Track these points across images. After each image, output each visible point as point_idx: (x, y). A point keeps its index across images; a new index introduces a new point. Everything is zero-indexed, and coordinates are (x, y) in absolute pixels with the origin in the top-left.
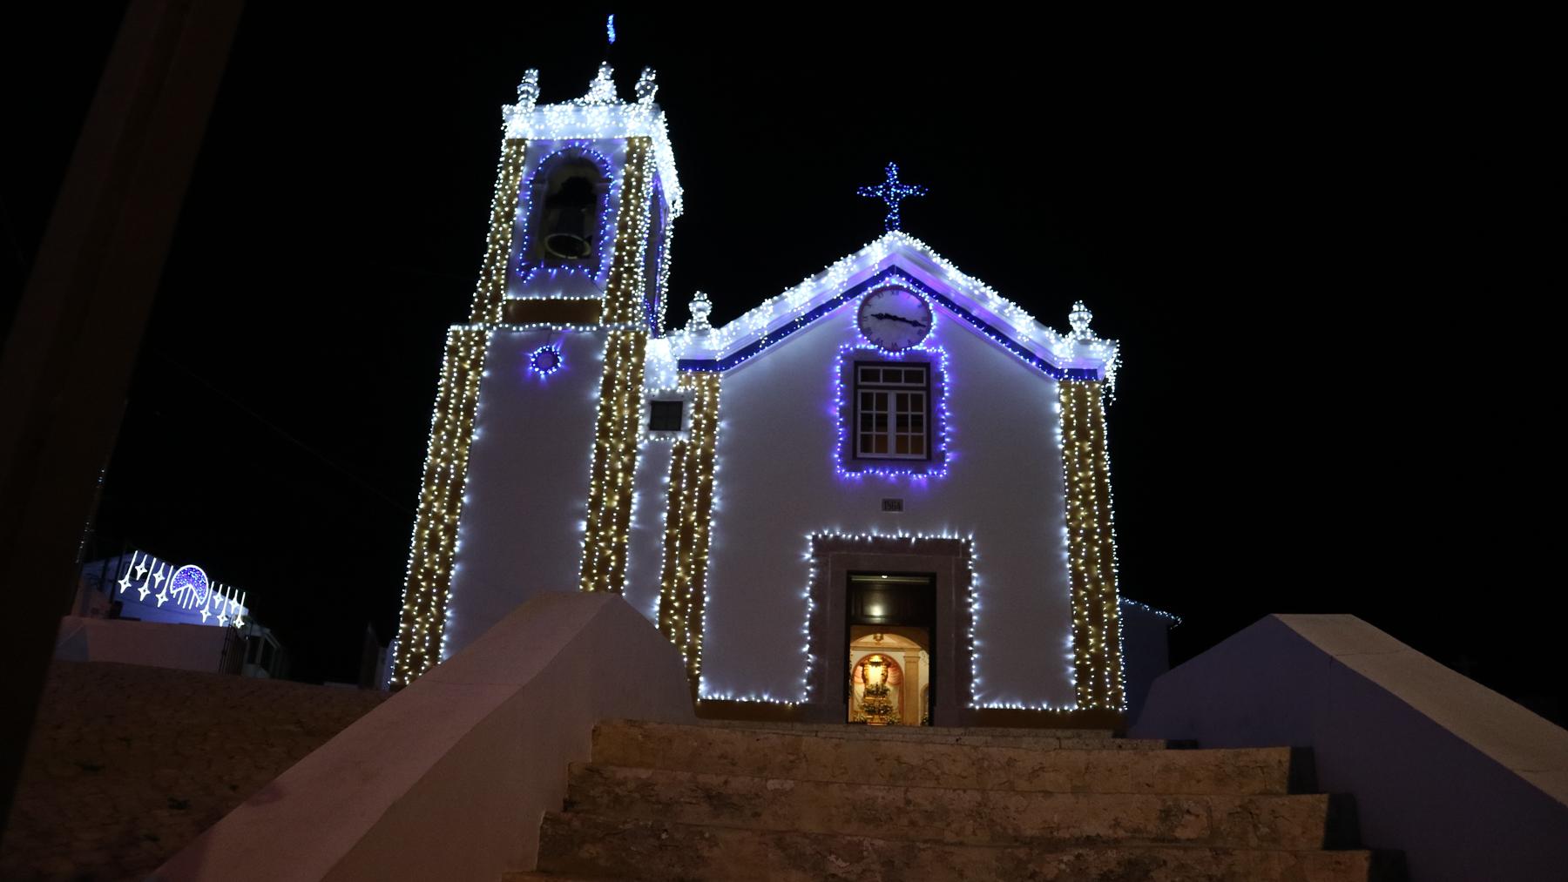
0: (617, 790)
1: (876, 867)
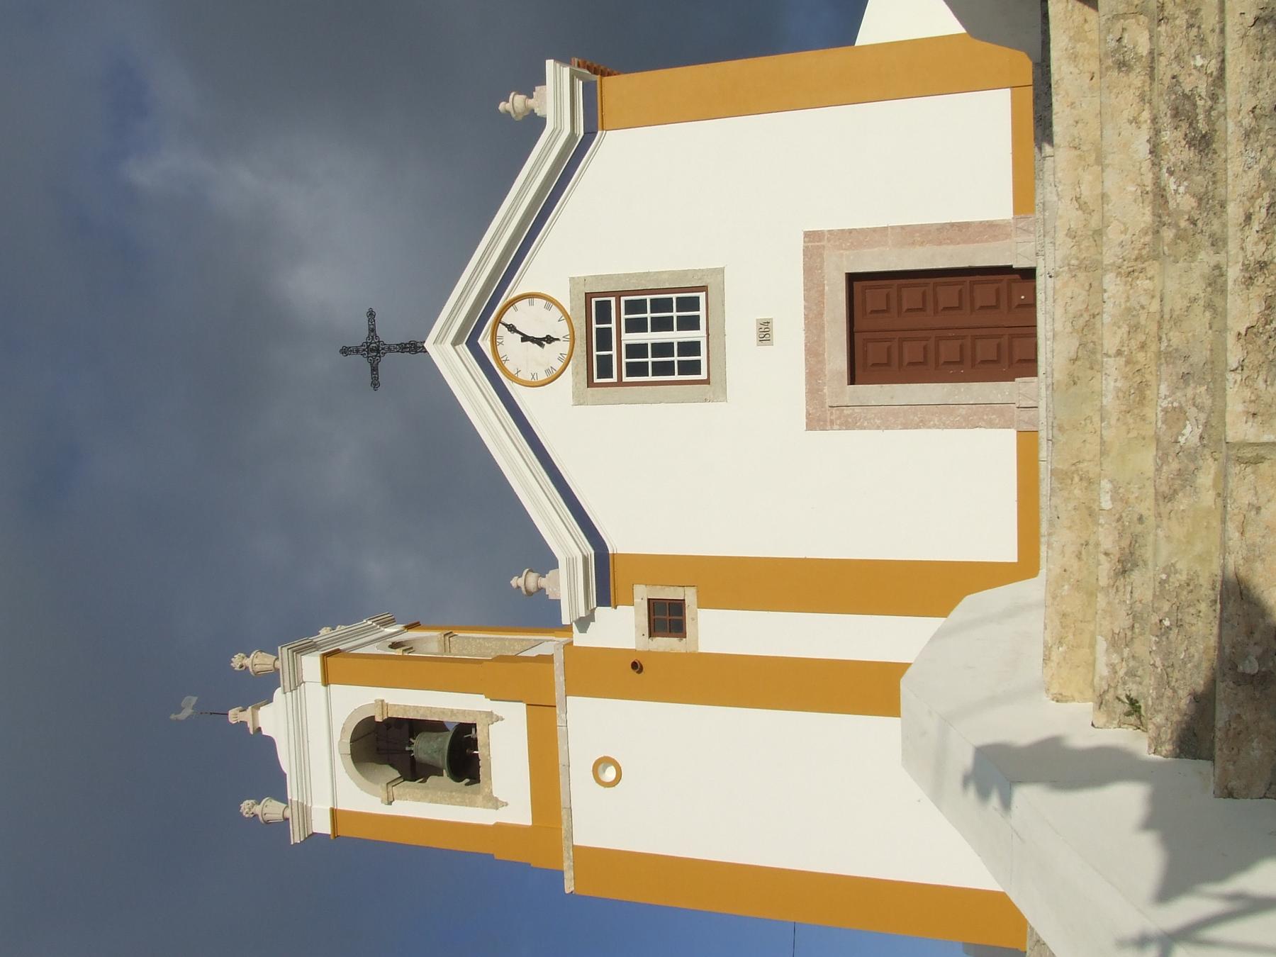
0: (1121, 673)
1: (1190, 392)
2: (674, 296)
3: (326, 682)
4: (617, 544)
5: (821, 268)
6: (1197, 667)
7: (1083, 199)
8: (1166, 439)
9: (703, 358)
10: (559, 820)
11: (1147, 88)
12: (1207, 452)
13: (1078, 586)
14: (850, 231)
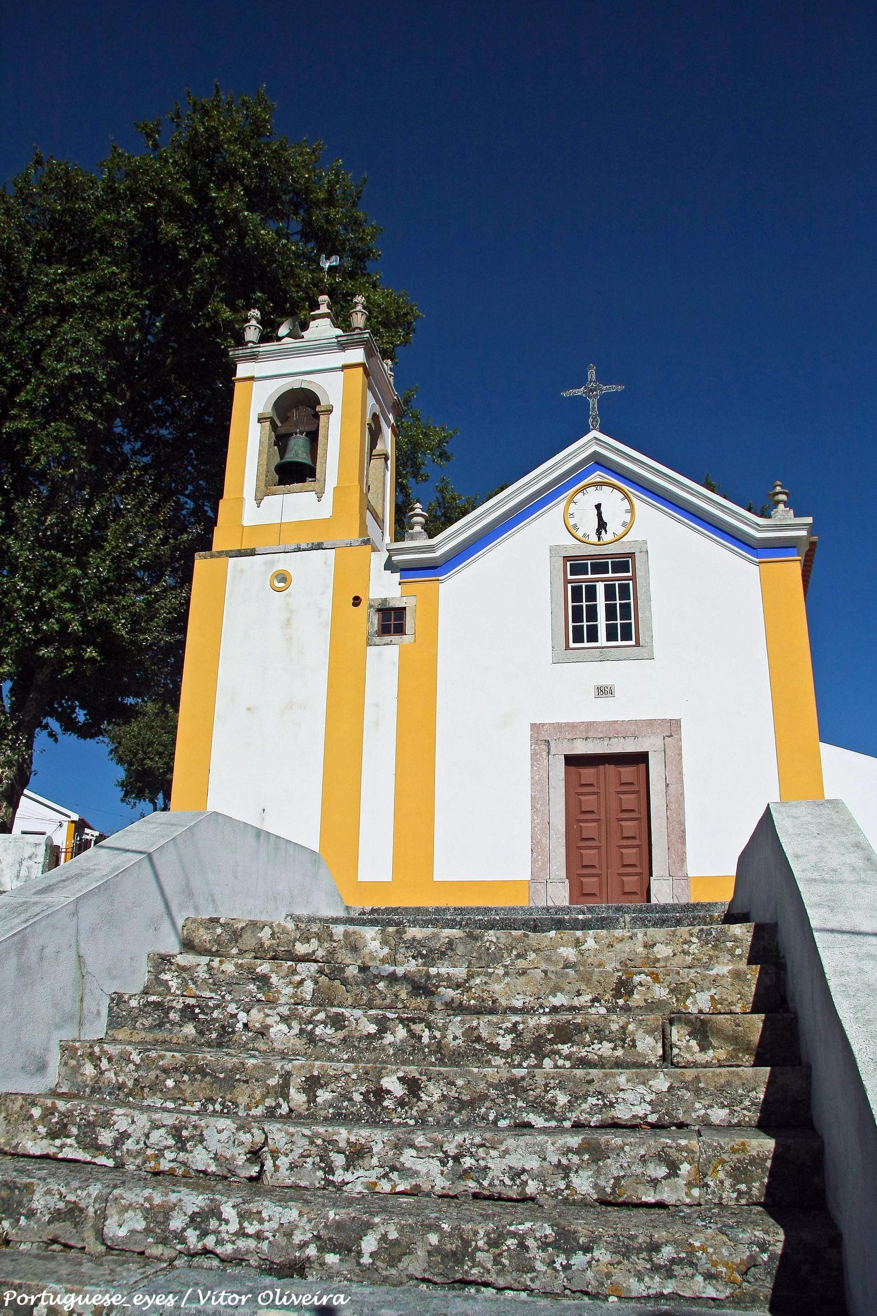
14: (680, 755)
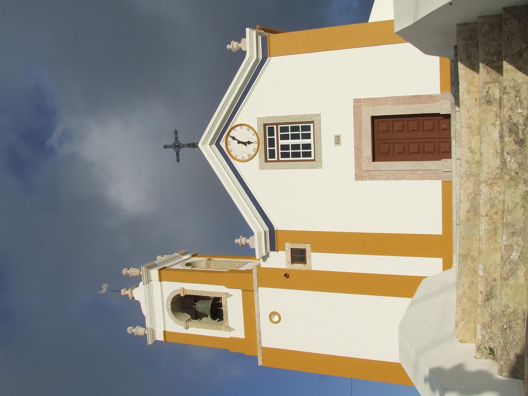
0: (487, 338)
1: (515, 239)
2: (300, 125)
3: (160, 280)
4: (277, 226)
5: (361, 114)
6: (517, 344)
7: (472, 148)
8: (505, 257)
9: (312, 150)
10: (255, 336)
11: (498, 112)
12: (521, 263)
13: (469, 299)
14: (373, 99)
